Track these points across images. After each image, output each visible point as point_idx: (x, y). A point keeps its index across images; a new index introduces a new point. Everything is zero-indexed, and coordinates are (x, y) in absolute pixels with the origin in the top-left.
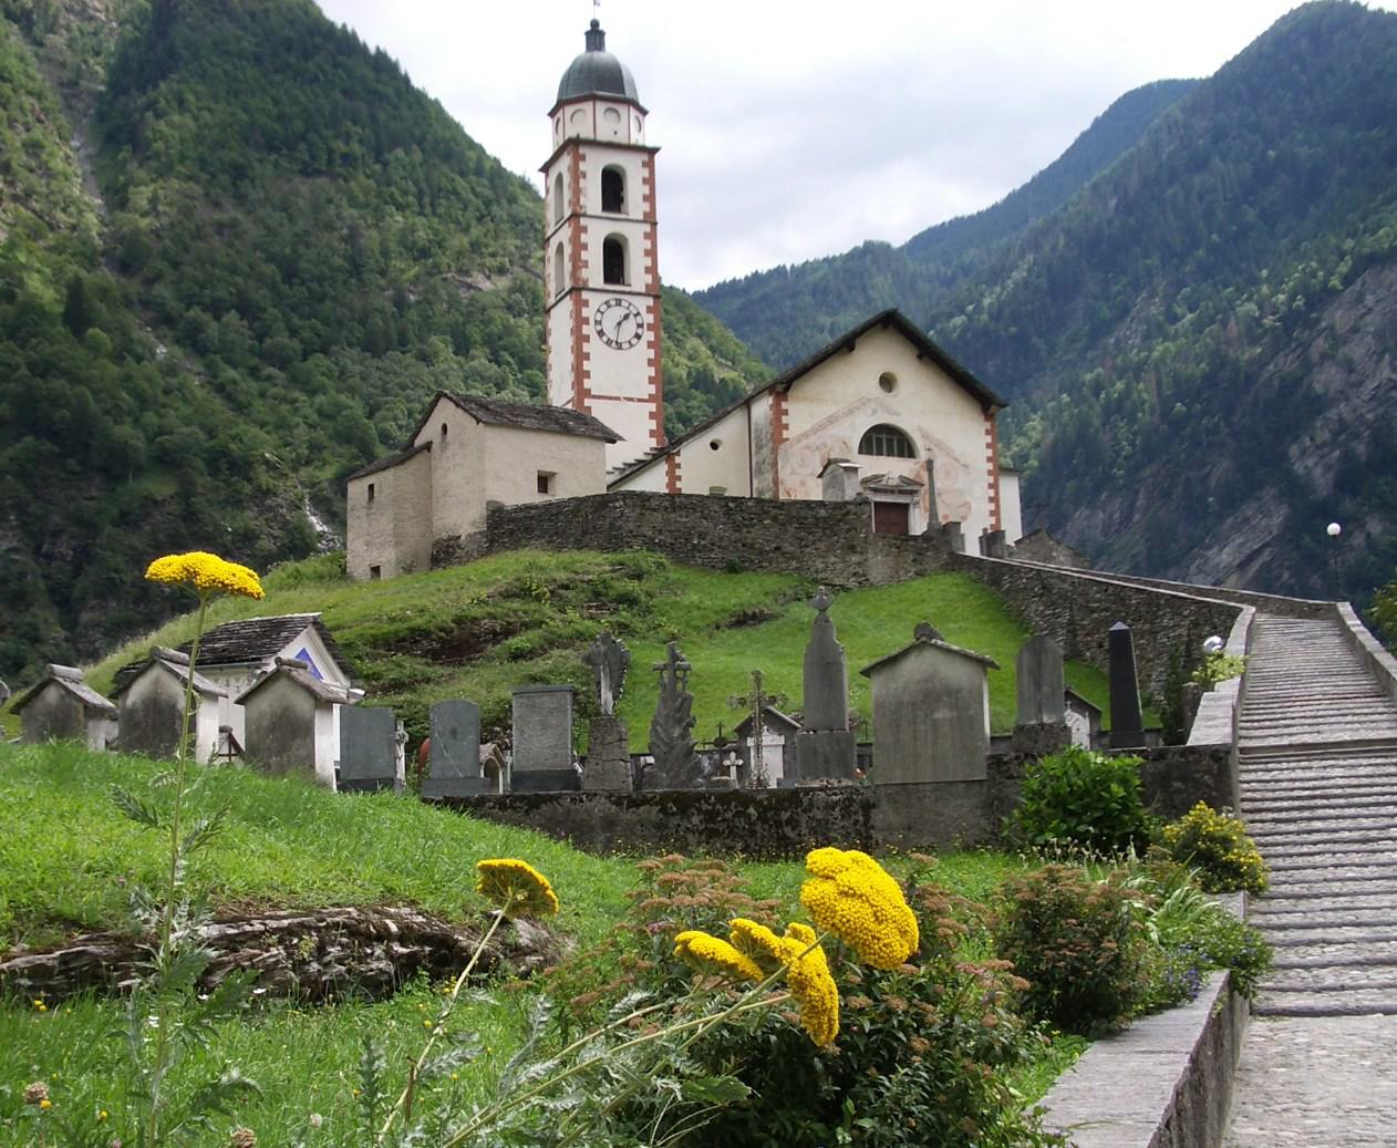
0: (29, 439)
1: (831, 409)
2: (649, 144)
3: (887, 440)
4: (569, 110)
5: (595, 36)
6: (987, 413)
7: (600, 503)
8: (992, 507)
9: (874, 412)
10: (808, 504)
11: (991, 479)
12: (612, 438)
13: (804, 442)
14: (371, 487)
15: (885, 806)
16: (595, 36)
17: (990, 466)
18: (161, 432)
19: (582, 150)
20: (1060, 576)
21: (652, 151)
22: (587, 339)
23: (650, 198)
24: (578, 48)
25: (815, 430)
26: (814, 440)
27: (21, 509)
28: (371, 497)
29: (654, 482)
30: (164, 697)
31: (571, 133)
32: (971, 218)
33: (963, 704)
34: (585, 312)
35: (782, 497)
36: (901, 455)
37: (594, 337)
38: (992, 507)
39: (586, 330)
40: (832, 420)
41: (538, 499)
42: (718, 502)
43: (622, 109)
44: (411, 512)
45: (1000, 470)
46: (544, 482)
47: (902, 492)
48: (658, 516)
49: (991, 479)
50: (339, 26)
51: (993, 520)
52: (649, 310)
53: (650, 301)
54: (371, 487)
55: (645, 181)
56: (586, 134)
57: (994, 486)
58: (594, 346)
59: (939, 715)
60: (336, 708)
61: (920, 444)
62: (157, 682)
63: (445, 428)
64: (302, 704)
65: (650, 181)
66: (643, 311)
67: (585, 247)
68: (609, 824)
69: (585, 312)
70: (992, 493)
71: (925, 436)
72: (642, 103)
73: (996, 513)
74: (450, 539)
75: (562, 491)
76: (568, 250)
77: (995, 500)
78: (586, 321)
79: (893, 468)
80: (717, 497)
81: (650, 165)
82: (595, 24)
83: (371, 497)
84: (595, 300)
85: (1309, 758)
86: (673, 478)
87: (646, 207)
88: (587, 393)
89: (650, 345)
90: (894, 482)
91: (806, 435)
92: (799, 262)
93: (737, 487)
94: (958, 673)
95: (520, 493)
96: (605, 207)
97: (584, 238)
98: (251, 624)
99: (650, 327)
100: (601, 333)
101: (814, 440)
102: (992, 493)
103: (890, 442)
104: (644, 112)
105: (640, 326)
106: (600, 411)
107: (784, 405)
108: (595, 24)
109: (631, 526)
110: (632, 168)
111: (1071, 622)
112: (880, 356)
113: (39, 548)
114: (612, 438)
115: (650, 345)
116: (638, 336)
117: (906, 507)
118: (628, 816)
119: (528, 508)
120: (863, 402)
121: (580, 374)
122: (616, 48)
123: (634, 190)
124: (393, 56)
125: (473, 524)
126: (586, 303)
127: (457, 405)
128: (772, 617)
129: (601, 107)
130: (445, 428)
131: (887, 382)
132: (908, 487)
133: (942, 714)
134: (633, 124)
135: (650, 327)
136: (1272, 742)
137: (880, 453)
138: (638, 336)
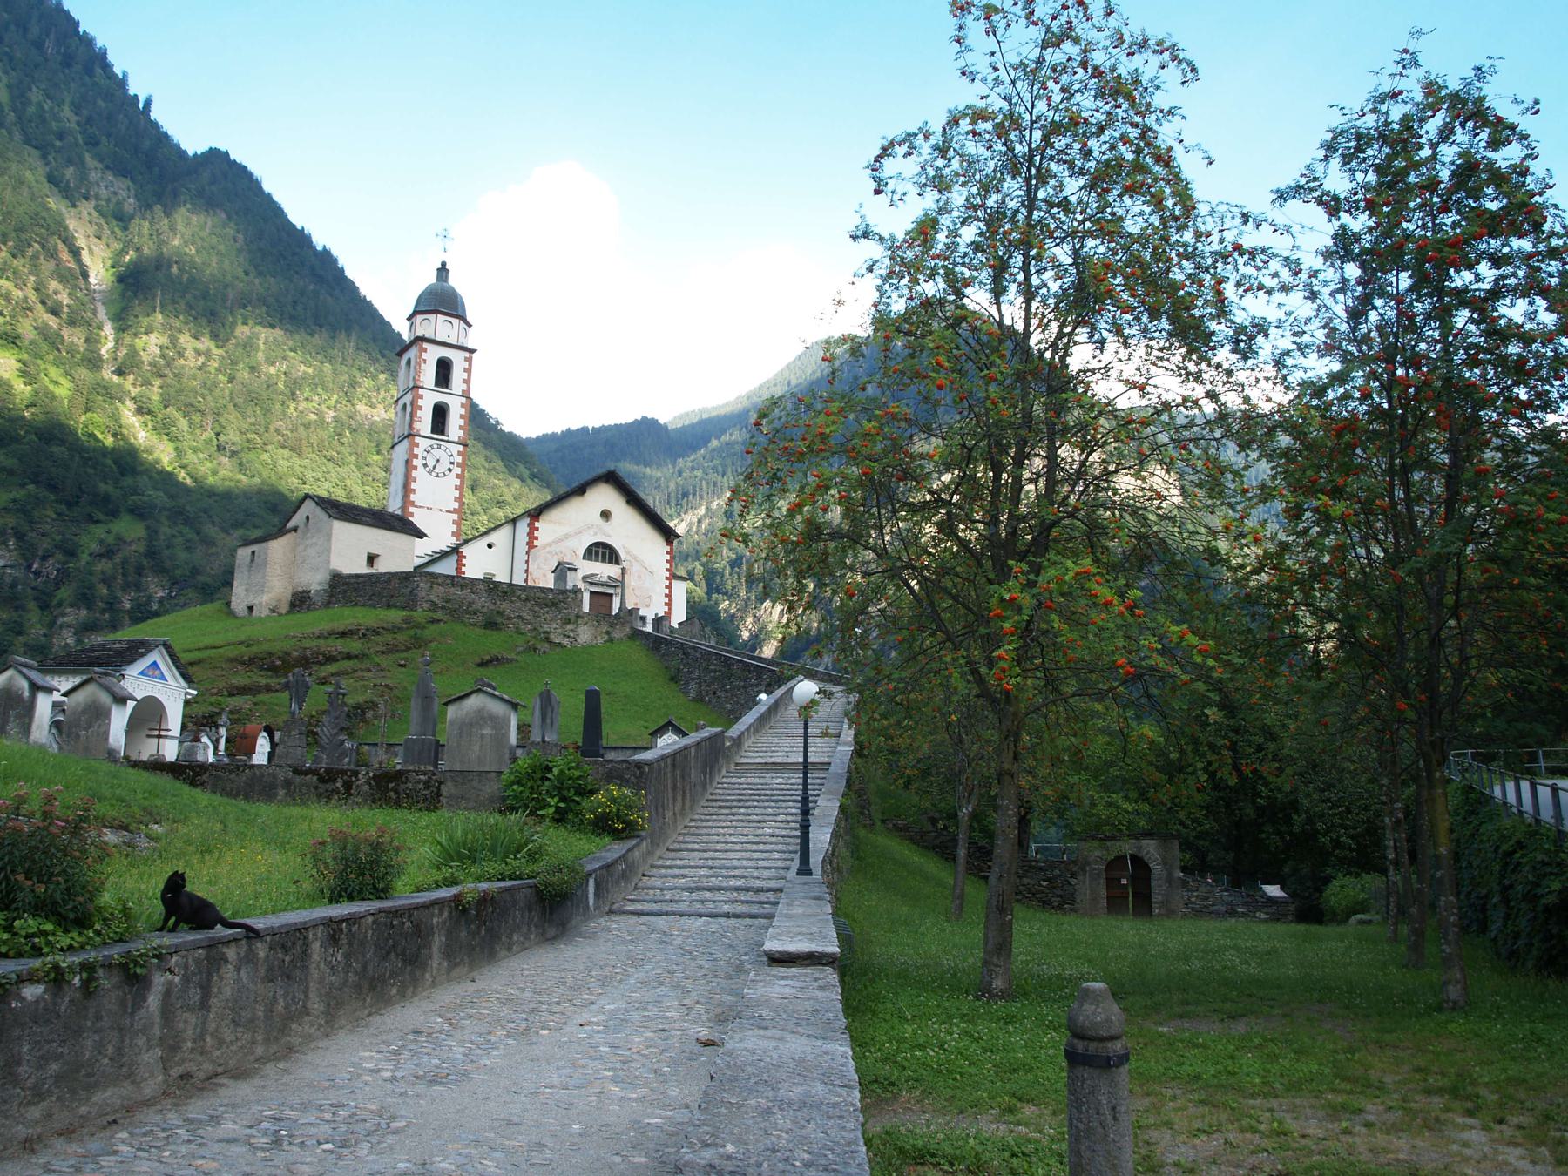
0: (31, 487)
1: (567, 530)
2: (470, 346)
3: (603, 552)
4: (420, 318)
5: (443, 271)
6: (669, 542)
7: (405, 577)
8: (667, 600)
9: (596, 534)
10: (542, 590)
11: (667, 583)
12: (420, 535)
13: (548, 549)
14: (253, 552)
15: (449, 784)
16: (443, 271)
17: (668, 574)
18: (135, 492)
19: (425, 345)
20: (694, 648)
21: (472, 351)
22: (415, 468)
23: (467, 382)
24: (432, 278)
25: (556, 542)
26: (554, 548)
27: (20, 536)
28: (252, 560)
29: (446, 568)
30: (15, 689)
31: (419, 333)
32: (628, 426)
33: (500, 724)
34: (416, 451)
35: (530, 583)
36: (611, 562)
37: (421, 467)
38: (667, 600)
39: (415, 462)
40: (567, 536)
41: (364, 570)
42: (489, 584)
43: (455, 321)
44: (279, 572)
45: (673, 576)
46: (371, 559)
47: (609, 586)
48: (442, 589)
49: (667, 583)
50: (299, 227)
51: (666, 609)
52: (459, 453)
53: (460, 448)
54: (253, 552)
55: (465, 370)
56: (429, 335)
57: (669, 587)
58: (420, 474)
59: (485, 732)
60: (131, 704)
61: (623, 556)
62: (11, 679)
63: (308, 518)
64: (105, 698)
65: (468, 370)
66: (455, 454)
67: (420, 408)
68: (287, 784)
69: (416, 451)
70: (667, 591)
71: (627, 552)
72: (469, 319)
73: (669, 604)
74: (304, 592)
75: (382, 567)
76: (409, 409)
77: (669, 596)
78: (416, 456)
79: (605, 570)
80: (488, 581)
81: (469, 360)
82: (444, 264)
83: (252, 560)
84: (424, 444)
85: (768, 771)
86: (460, 564)
87: (464, 387)
88: (412, 504)
89: (458, 476)
90: (605, 579)
91: (549, 545)
92: (597, 425)
93: (502, 577)
94: (498, 708)
95: (354, 565)
96: (437, 384)
97: (420, 402)
98: (120, 642)
99: (459, 465)
100: (425, 465)
101: (554, 548)
102: (667, 591)
103: (604, 555)
104: (470, 325)
105: (452, 463)
106: (418, 519)
107: (537, 524)
108: (444, 264)
109: (424, 594)
110: (457, 358)
111: (699, 678)
112: (604, 497)
113: (30, 567)
114: (420, 535)
115: (458, 476)
116: (450, 470)
117: (611, 595)
118: (298, 779)
119: (358, 576)
120: (590, 527)
121: (407, 489)
122: (454, 281)
123: (457, 375)
124: (335, 253)
125: (320, 584)
126: (417, 445)
127: (317, 504)
128: (510, 661)
129: (441, 318)
130: (308, 518)
131: (606, 515)
132: (612, 583)
133: (487, 731)
134: (462, 331)
135: (459, 465)
136: (757, 761)
137: (604, 561)
138: (450, 470)
